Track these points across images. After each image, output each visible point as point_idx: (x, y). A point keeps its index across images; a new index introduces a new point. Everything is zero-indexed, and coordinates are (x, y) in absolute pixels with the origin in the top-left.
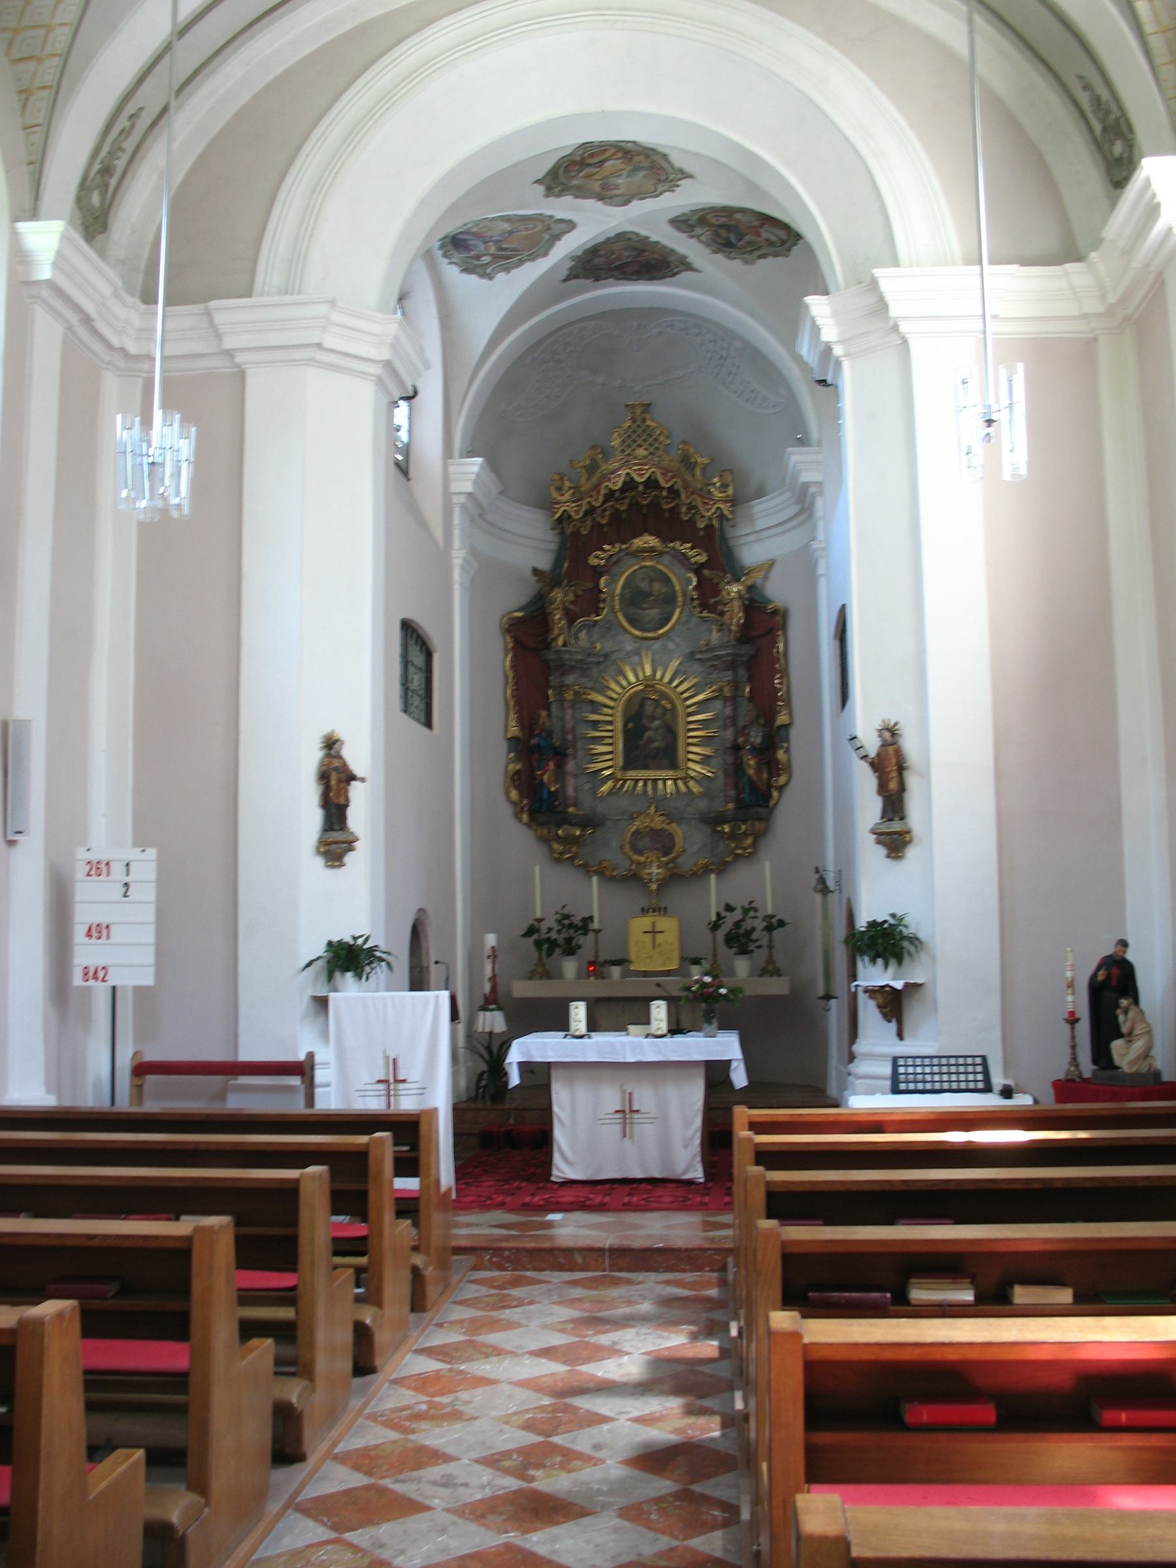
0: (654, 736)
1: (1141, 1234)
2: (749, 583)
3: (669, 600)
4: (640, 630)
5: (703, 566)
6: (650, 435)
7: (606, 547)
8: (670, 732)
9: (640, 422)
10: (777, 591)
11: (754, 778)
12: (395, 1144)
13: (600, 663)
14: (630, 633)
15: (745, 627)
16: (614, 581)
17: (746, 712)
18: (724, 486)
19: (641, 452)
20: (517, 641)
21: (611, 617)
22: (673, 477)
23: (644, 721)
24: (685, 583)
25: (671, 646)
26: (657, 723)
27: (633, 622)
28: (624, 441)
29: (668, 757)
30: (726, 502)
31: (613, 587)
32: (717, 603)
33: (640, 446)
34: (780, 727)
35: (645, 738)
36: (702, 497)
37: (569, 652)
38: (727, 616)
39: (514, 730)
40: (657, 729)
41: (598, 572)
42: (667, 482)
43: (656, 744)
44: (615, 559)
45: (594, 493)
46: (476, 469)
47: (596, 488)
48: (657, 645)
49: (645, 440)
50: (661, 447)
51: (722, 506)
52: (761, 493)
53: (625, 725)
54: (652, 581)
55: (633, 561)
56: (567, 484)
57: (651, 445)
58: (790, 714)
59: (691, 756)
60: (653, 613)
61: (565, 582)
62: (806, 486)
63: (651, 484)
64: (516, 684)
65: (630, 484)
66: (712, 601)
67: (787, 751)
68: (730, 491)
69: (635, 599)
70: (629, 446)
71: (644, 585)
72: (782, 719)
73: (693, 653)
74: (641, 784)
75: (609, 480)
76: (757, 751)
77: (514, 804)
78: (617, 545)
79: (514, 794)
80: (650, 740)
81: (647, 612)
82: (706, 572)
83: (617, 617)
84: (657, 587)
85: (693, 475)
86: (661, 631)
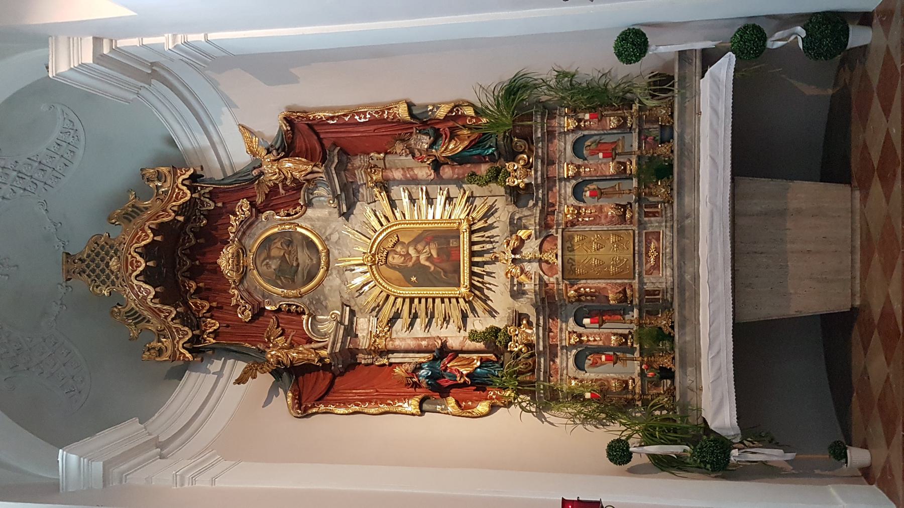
0: (424, 255)
1: (707, 186)
2: (264, 153)
3: (289, 240)
4: (318, 270)
5: (253, 204)
6: (98, 254)
7: (234, 302)
8: (428, 236)
9: (87, 264)
10: (271, 127)
11: (466, 143)
12: (531, 126)
13: (353, 313)
14: (322, 280)
15: (310, 156)
16: (266, 295)
17: (400, 162)
18: (159, 176)
19: (113, 263)
20: (320, 399)
21: (306, 299)
22: (143, 230)
23: (410, 264)
24: (272, 224)
25: (335, 237)
26: (412, 251)
27: (311, 278)
28: (104, 282)
29: (444, 238)
30: (175, 174)
31: (277, 295)
32: (285, 186)
33: (107, 265)
34: (411, 114)
35: (427, 264)
36: (169, 201)
37: (333, 343)
38: (297, 175)
39: (411, 406)
40: (418, 252)
41: (259, 312)
42: (147, 235)
43: (435, 255)
44: (245, 294)
45: (162, 315)
46: (73, 458)
47: (156, 312)
48: (334, 252)
49: (102, 260)
50: (110, 243)
51: (180, 180)
52: (171, 142)
53: (415, 285)
54: (269, 257)
55: (249, 275)
56: (154, 344)
57: (107, 254)
58: (398, 102)
59: (446, 216)
60: (303, 257)
61: (261, 346)
62: (99, 58)
63: (147, 252)
64: (363, 401)
65: (148, 276)
66: (282, 191)
67: (437, 106)
68: (164, 170)
69: (287, 274)
70: (108, 277)
71: (274, 264)
72: (402, 112)
73: (342, 214)
74: (476, 269)
75: (145, 298)
76: (437, 137)
77: (493, 408)
78: (232, 291)
79: (483, 407)
80: (430, 258)
81: (300, 261)
82: (259, 200)
83: (306, 292)
84: (275, 252)
85: (147, 209)
86: (320, 248)
